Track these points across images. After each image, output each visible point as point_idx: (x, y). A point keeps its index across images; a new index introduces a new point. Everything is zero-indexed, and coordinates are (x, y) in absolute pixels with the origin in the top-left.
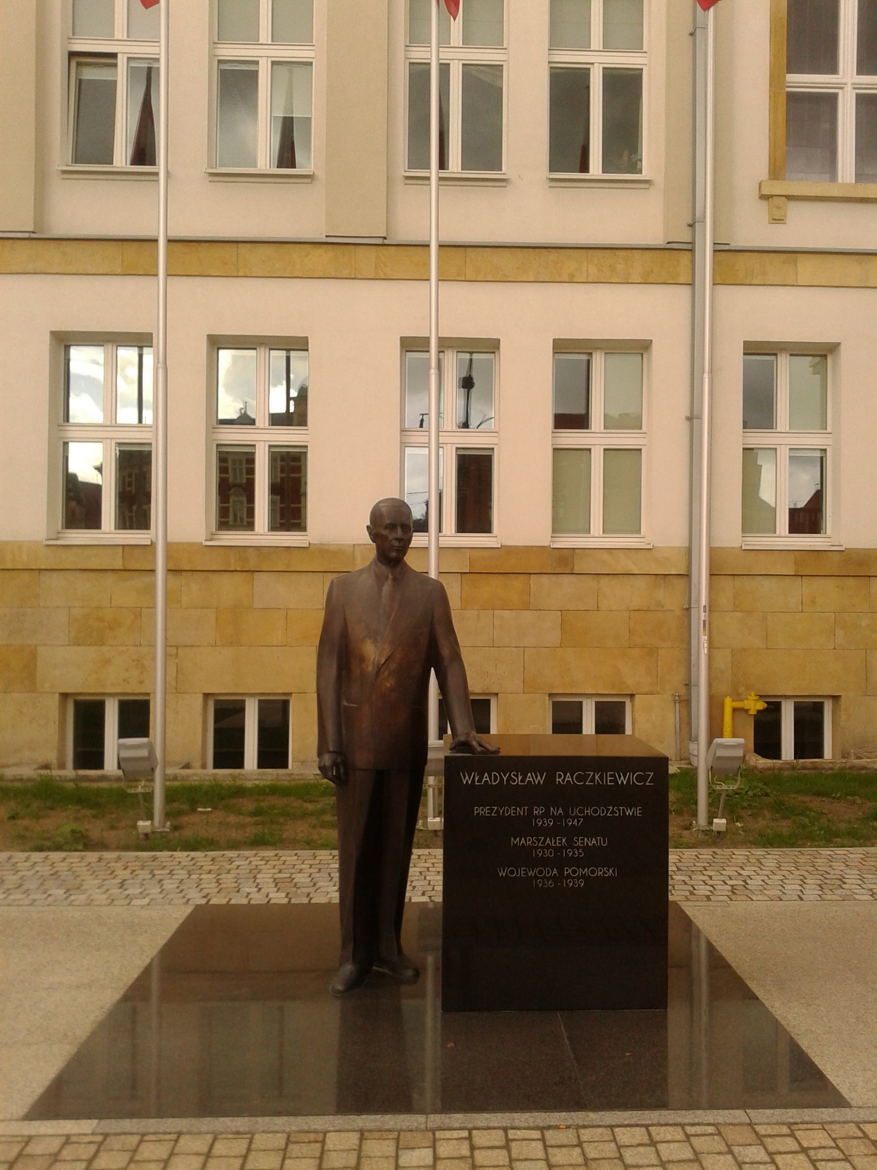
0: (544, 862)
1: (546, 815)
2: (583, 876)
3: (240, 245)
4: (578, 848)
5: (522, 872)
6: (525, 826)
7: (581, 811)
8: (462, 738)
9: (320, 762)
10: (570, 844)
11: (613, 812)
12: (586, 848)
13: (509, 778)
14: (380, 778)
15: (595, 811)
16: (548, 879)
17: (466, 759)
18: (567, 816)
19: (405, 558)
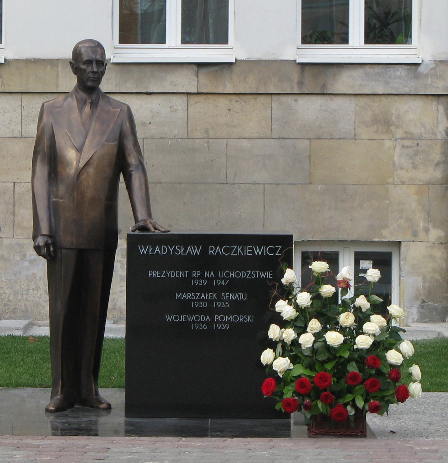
0: (201, 311)
1: (201, 277)
2: (229, 322)
3: (273, 96)
4: (225, 301)
5: (183, 318)
6: (185, 285)
7: (228, 274)
8: (141, 224)
9: (35, 244)
10: (219, 298)
11: (251, 275)
12: (231, 302)
13: (175, 250)
14: (81, 254)
15: (238, 274)
16: (203, 323)
17: (142, 237)
18: (217, 277)
19: (99, 86)
